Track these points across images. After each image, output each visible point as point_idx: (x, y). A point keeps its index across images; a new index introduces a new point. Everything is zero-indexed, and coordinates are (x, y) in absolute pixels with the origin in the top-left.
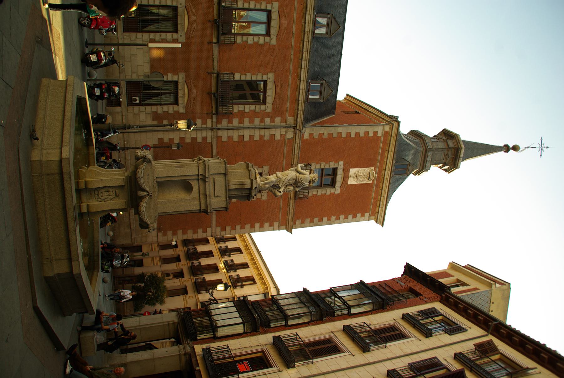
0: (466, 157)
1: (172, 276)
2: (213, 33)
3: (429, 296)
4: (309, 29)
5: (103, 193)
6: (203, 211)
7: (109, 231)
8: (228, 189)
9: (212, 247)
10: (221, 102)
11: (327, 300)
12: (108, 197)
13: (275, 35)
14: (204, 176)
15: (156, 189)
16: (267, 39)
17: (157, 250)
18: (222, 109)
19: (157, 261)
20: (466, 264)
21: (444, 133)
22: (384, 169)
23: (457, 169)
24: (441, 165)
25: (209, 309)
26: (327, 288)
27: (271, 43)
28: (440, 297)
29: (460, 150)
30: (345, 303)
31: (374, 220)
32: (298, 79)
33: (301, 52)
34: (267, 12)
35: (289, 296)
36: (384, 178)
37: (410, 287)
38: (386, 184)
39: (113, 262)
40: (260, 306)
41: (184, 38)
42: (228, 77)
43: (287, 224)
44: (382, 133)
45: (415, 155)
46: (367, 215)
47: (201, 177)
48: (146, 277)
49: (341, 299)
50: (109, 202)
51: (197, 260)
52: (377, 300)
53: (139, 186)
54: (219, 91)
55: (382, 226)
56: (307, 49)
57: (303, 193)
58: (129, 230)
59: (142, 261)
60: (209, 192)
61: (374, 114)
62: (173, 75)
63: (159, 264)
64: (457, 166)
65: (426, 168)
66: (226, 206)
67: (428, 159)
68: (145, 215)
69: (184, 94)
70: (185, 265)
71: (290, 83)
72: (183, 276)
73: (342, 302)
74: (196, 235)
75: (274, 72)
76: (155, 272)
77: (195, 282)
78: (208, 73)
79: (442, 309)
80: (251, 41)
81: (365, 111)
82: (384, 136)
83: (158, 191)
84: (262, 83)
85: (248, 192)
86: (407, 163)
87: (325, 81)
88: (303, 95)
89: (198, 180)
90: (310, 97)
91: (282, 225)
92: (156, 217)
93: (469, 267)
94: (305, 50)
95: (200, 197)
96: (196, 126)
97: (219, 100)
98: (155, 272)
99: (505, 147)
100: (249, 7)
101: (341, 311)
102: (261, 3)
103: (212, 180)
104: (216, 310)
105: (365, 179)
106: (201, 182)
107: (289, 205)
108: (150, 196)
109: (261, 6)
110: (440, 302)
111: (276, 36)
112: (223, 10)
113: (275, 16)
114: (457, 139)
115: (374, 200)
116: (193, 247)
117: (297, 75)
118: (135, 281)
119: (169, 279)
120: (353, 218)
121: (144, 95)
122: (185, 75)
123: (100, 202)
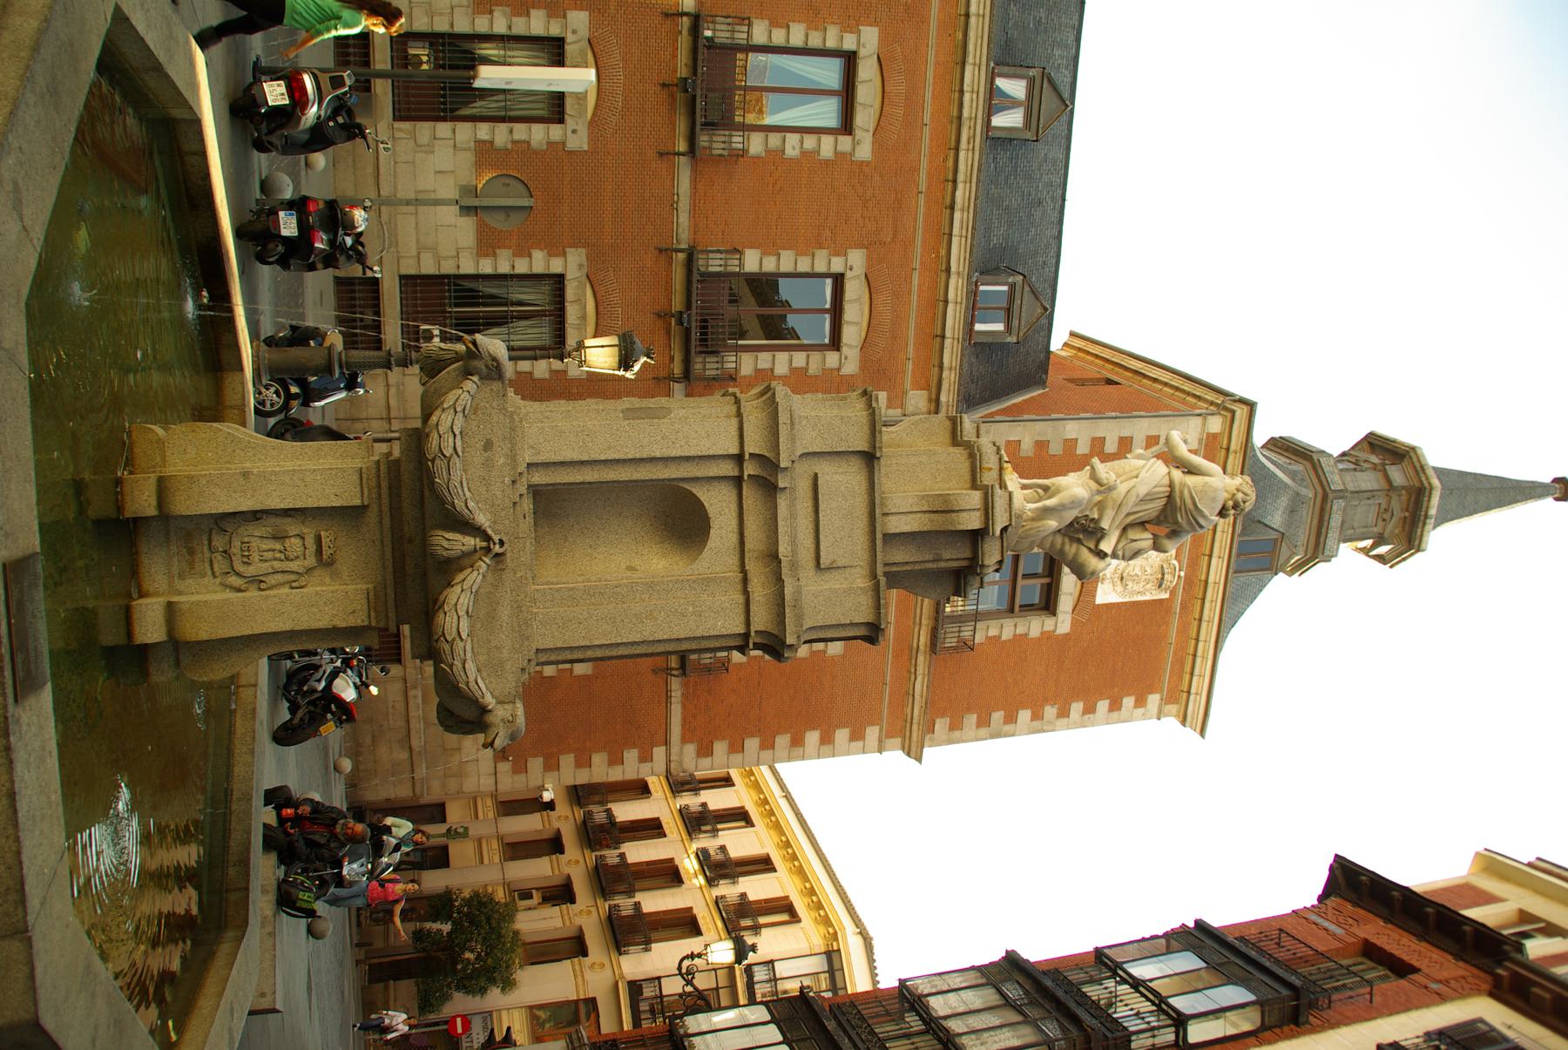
0: (1445, 517)
1: (536, 895)
3: (1446, 974)
4: (974, 111)
5: (255, 543)
6: (758, 640)
7: (340, 756)
8: (878, 537)
9: (659, 805)
10: (701, 340)
11: (1092, 991)
12: (277, 565)
14: (770, 464)
15: (526, 525)
16: (845, 142)
17: (491, 815)
18: (704, 363)
19: (493, 852)
20: (1532, 859)
21: (1371, 444)
22: (1207, 552)
23: (1419, 554)
24: (1368, 543)
25: (682, 1031)
26: (1083, 944)
27: (856, 155)
28: (1489, 978)
29: (1427, 492)
30: (1164, 1006)
31: (1177, 716)
32: (942, 271)
35: (958, 980)
36: (1206, 582)
37: (1366, 941)
38: (1212, 601)
39: (341, 867)
40: (863, 1019)
42: (722, 262)
43: (908, 734)
44: (1200, 440)
45: (1292, 511)
46: (1154, 700)
47: (750, 469)
48: (457, 904)
49: (1141, 989)
50: (286, 590)
51: (616, 848)
52: (1276, 995)
53: (441, 501)
54: (694, 308)
55: (1202, 733)
57: (957, 634)
58: (404, 755)
59: (445, 849)
60: (793, 542)
61: (1166, 384)
62: (550, 255)
63: (496, 859)
64: (1420, 544)
65: (1327, 553)
66: (870, 618)
67: (1332, 524)
68: (469, 655)
69: (584, 317)
70: (577, 862)
71: (916, 282)
72: (572, 899)
73: (1148, 999)
74: (619, 768)
76: (486, 886)
77: (610, 917)
78: (661, 251)
79: (1510, 1027)
80: (794, 148)
81: (1136, 377)
82: (1205, 449)
83: (537, 539)
84: (829, 281)
85: (967, 554)
86: (1274, 535)
87: (1021, 277)
89: (738, 481)
90: (978, 327)
91: (890, 735)
92: (523, 670)
93: (1540, 865)
94: (961, 177)
95: (743, 571)
96: (652, 358)
97: (695, 335)
98: (486, 886)
99: (1557, 486)
101: (1154, 1036)
102: (825, 29)
103: (804, 487)
104: (708, 1036)
105: (1148, 586)
106: (750, 495)
107: (913, 670)
108: (497, 555)
109: (824, 39)
110: (1492, 995)
111: (871, 133)
112: (709, 48)
113: (867, 71)
114: (1415, 460)
115: (1175, 653)
116: (601, 809)
117: (938, 256)
118: (422, 912)
119: (530, 909)
120: (1111, 710)
121: (456, 319)
122: (587, 258)
123: (239, 590)
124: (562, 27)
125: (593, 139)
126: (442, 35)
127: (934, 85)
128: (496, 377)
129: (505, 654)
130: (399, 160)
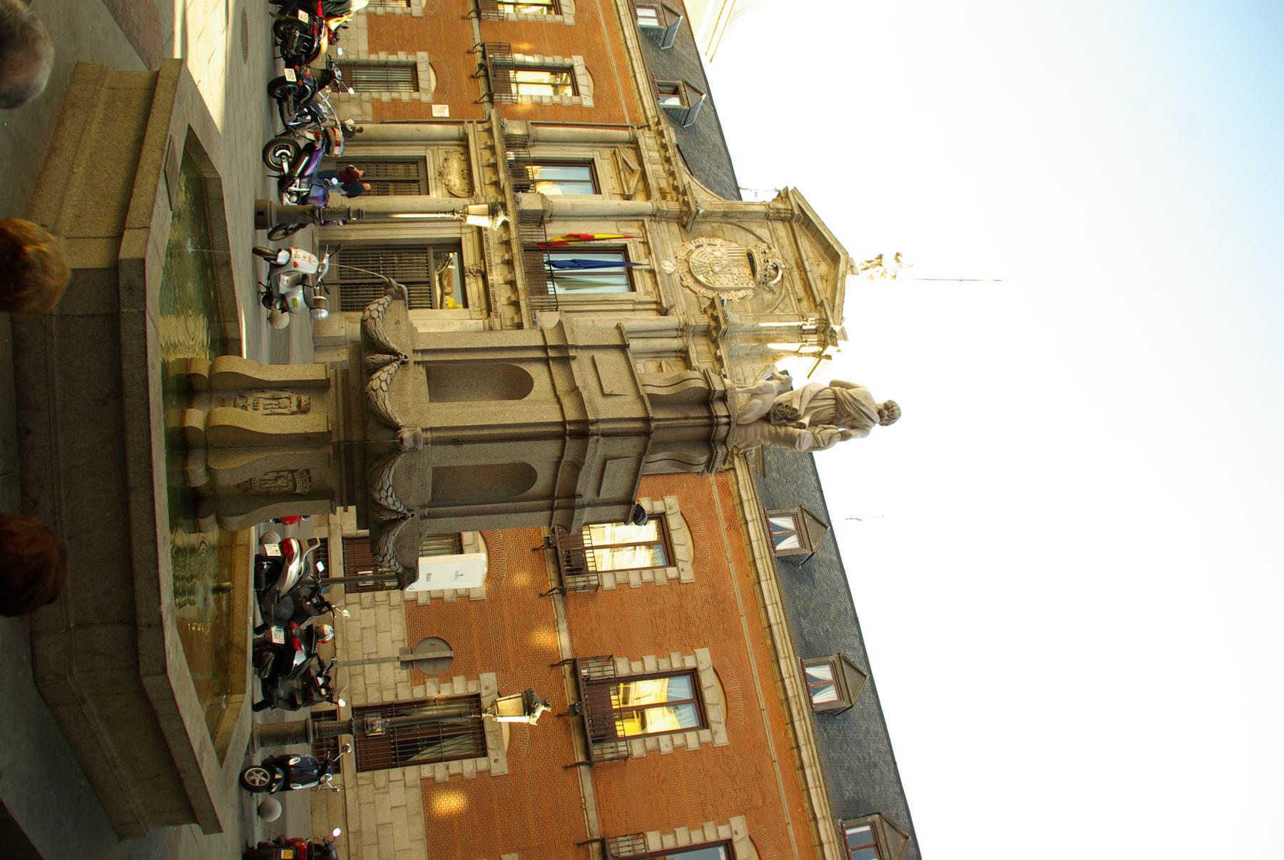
2: (572, 743)
5: (261, 401)
13: (720, 723)
16: (705, 735)
32: (810, 820)
33: (795, 750)
34: (689, 677)
41: (506, 766)
42: (630, 848)
56: (807, 738)
75: (745, 814)
78: (579, 845)
80: (667, 746)
84: (721, 850)
87: (877, 816)
88: (835, 856)
94: (801, 742)
100: (644, 669)
102: (670, 656)
109: (671, 663)
111: (723, 724)
113: (708, 679)
117: (803, 810)
124: (477, 686)
125: (511, 764)
126: (390, 705)
127: (760, 681)
128: (401, 297)
129: (409, 405)
130: (363, 802)
